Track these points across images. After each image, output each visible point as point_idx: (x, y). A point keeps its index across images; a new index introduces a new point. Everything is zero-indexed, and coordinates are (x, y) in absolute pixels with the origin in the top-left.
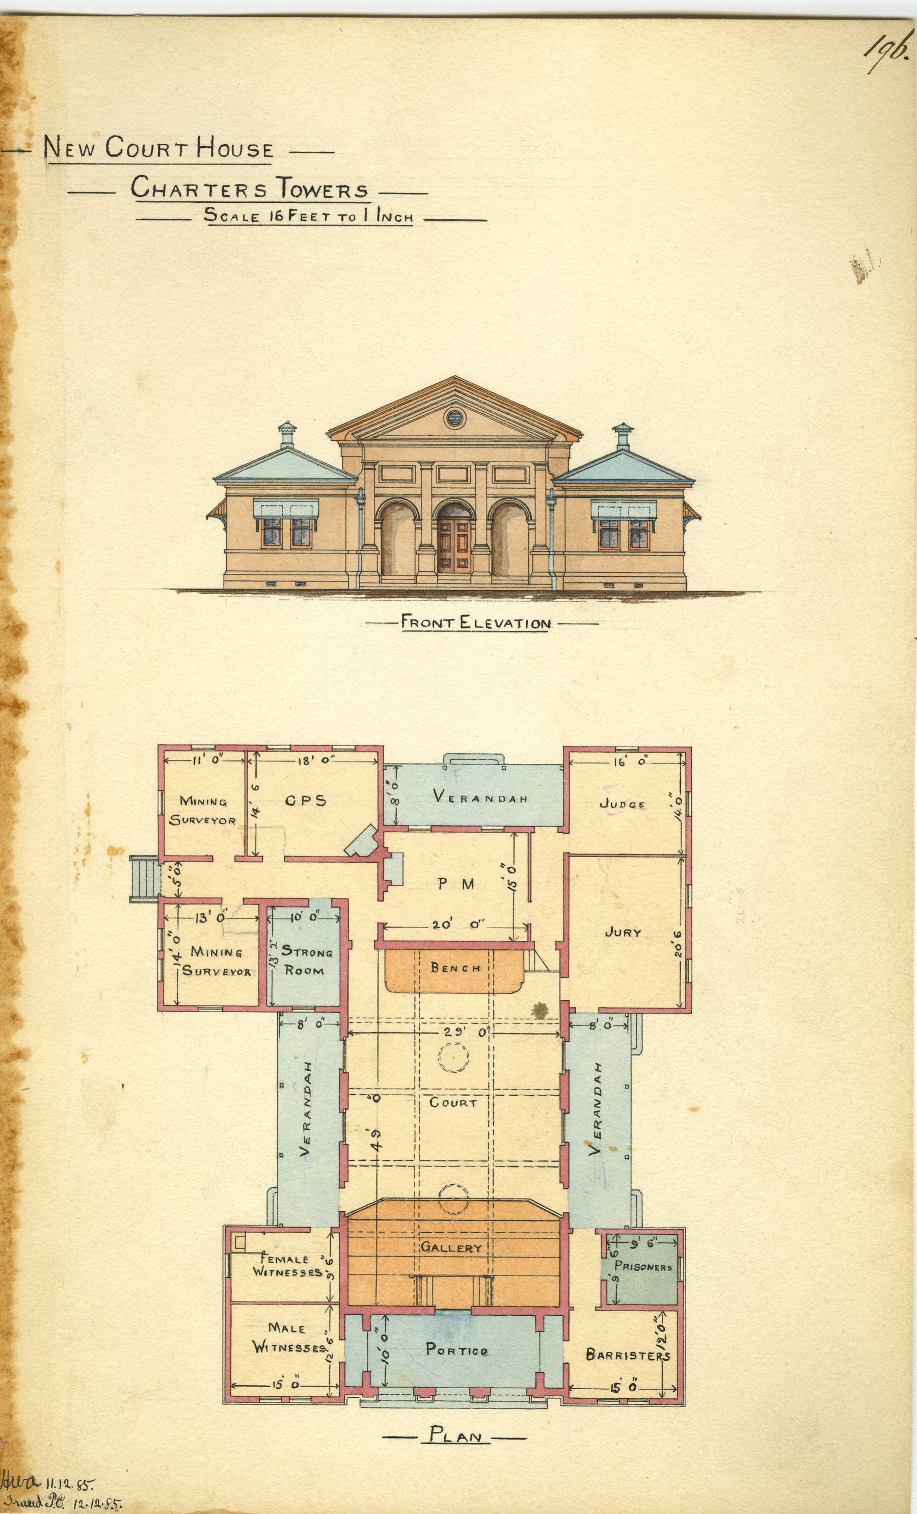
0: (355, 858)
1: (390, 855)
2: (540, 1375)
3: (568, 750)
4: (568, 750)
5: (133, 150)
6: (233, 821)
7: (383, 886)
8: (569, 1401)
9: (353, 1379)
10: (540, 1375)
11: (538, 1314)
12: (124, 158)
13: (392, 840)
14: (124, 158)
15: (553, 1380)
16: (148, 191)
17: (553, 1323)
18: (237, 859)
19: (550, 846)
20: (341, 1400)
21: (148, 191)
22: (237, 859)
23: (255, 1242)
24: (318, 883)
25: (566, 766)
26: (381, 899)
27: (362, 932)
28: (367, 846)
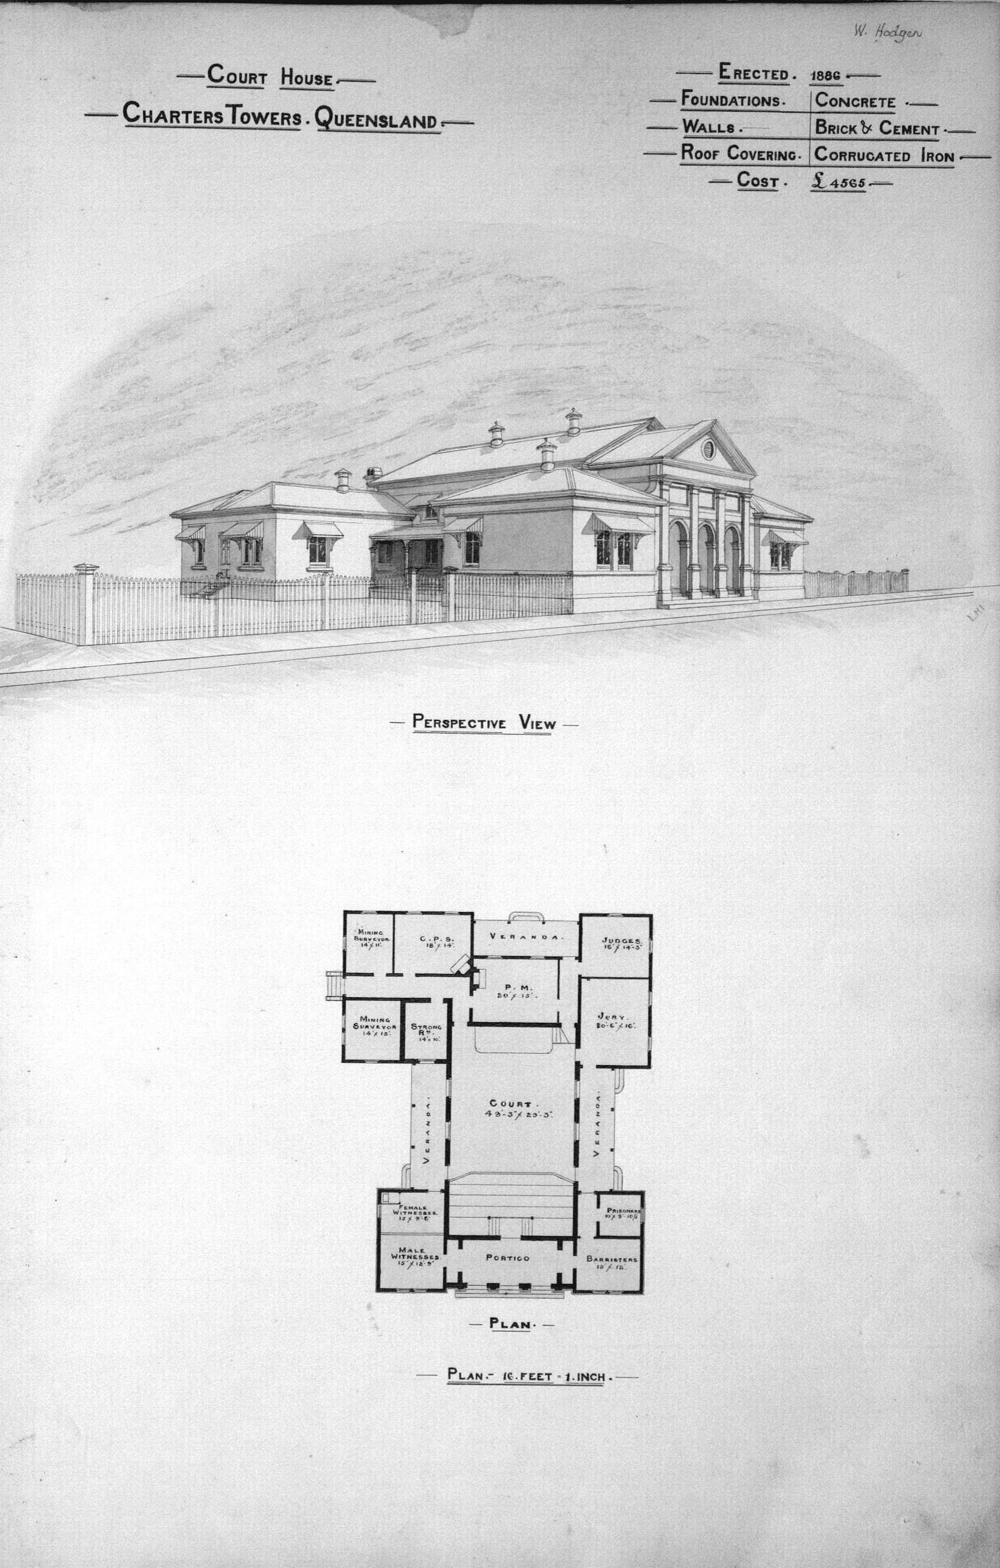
0: (458, 974)
1: (478, 971)
2: (559, 1276)
3: (581, 915)
4: (581, 915)
5: (834, 156)
6: (394, 1027)
7: (473, 988)
8: (576, 1292)
9: (452, 1278)
10: (559, 1276)
11: (560, 1240)
12: (750, 186)
13: (477, 963)
14: (750, 186)
15: (567, 1279)
16: (222, 78)
17: (568, 1245)
18: (388, 975)
19: (571, 969)
20: (443, 1291)
21: (222, 78)
22: (388, 975)
23: (394, 1197)
24: (437, 989)
25: (580, 923)
26: (471, 994)
27: (460, 1016)
28: (465, 969)
